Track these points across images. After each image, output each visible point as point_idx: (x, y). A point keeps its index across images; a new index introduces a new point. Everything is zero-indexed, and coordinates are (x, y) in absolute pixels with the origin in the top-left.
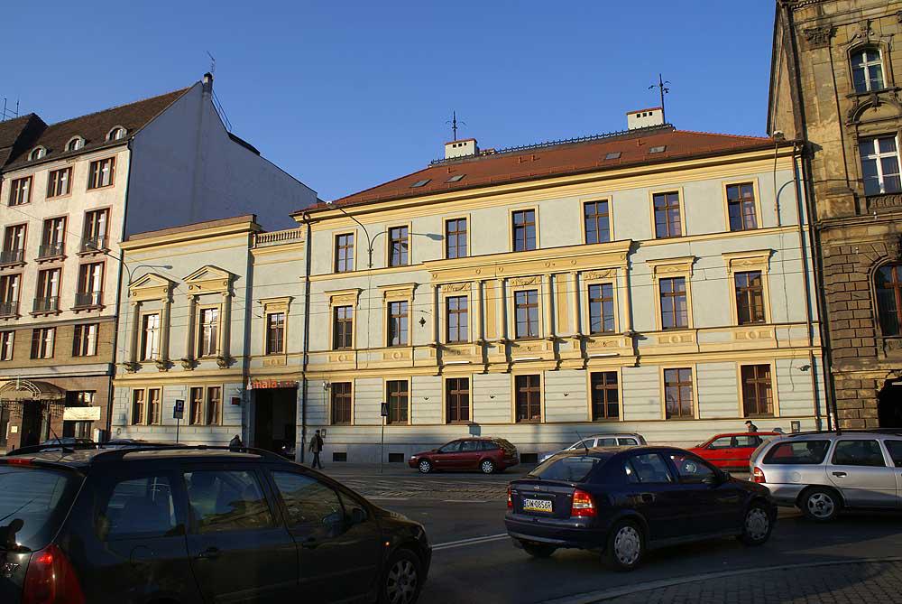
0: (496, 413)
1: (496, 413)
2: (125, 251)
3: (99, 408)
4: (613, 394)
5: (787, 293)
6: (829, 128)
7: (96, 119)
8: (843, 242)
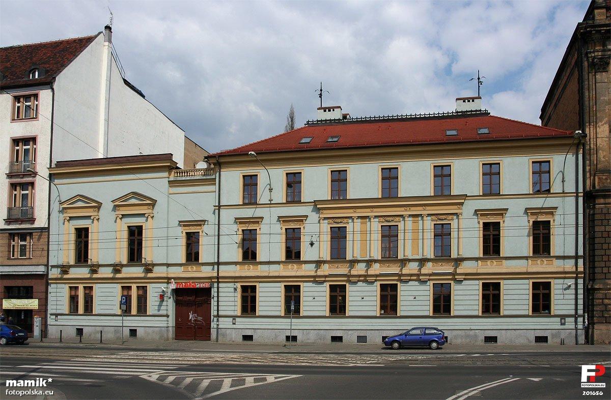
0: (364, 308)
1: (364, 308)
2: (548, 163)
3: (37, 300)
4: (254, 299)
5: (566, 237)
6: (602, 128)
7: (62, 46)
8: (604, 206)
